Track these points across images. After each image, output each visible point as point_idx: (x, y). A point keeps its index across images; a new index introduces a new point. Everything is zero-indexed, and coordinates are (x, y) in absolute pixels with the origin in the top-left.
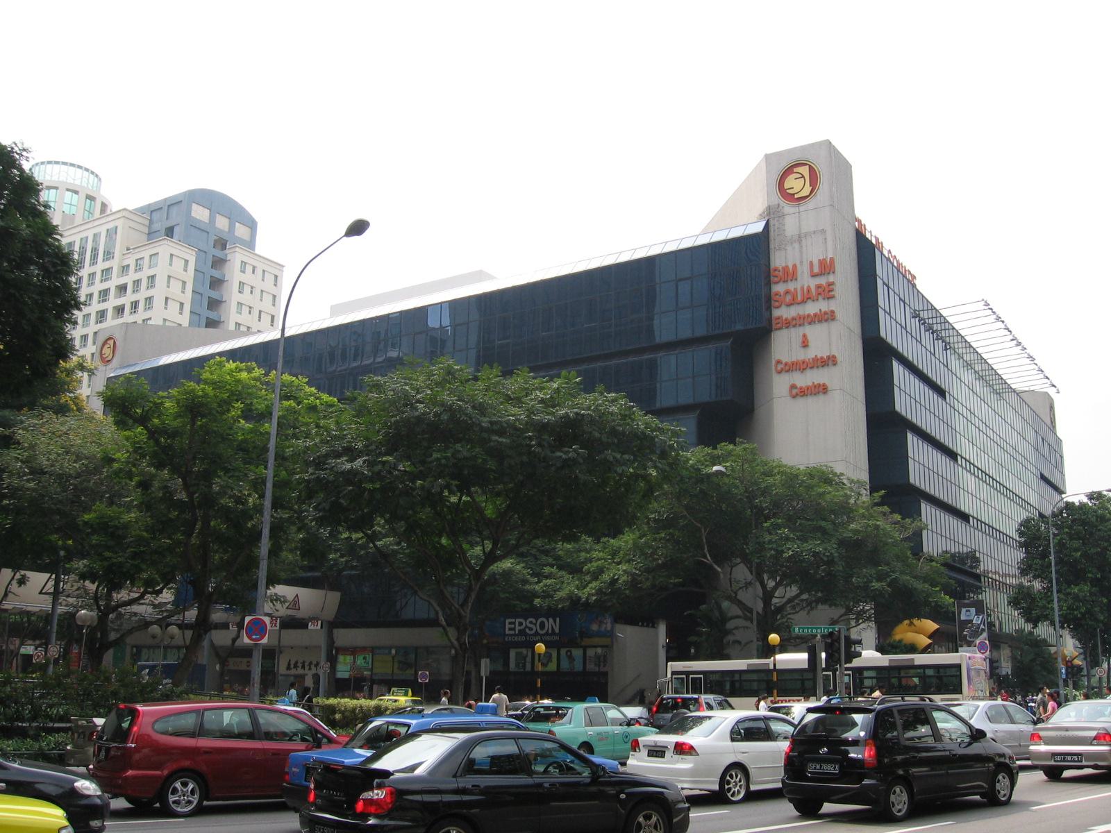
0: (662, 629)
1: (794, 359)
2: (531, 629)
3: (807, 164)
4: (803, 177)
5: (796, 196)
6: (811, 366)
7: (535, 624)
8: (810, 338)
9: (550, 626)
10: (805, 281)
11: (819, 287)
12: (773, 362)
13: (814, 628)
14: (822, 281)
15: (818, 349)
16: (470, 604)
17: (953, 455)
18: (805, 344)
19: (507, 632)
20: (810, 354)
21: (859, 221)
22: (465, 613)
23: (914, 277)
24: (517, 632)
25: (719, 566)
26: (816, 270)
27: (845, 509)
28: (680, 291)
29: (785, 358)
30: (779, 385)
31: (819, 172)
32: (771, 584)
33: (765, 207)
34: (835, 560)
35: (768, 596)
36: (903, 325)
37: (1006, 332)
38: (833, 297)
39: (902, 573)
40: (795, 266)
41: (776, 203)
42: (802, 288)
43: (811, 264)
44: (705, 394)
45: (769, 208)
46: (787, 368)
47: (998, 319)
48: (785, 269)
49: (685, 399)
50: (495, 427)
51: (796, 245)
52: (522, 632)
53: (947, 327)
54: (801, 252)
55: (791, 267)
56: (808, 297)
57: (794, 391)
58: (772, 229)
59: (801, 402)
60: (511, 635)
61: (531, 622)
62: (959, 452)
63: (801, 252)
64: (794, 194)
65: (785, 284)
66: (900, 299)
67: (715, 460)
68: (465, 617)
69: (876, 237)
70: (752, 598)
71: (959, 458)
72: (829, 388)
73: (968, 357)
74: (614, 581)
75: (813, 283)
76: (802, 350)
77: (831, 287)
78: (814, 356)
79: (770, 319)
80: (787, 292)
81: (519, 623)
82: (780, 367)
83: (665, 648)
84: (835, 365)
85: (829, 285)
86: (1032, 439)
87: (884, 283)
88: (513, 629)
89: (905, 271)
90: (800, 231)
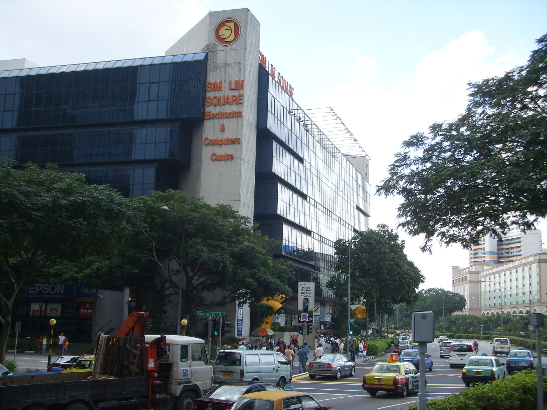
0: (127, 291)
1: (216, 138)
2: (46, 291)
3: (233, 21)
4: (231, 29)
5: (225, 40)
6: (226, 143)
7: (48, 288)
8: (225, 126)
9: (58, 290)
10: (226, 92)
11: (234, 96)
12: (204, 138)
13: (208, 313)
14: (236, 93)
15: (229, 134)
16: (13, 299)
17: (304, 196)
18: (223, 130)
19: (30, 292)
20: (225, 136)
21: (262, 55)
22: (10, 303)
23: (292, 89)
24: (36, 292)
25: (161, 263)
26: (233, 86)
27: (238, 232)
28: (151, 91)
29: (211, 137)
30: (207, 152)
31: (240, 28)
32: (191, 274)
33: (206, 44)
34: (227, 265)
35: (189, 280)
36: (282, 121)
37: (342, 125)
38: (241, 104)
39: (264, 273)
40: (221, 82)
41: (214, 43)
42: (224, 96)
43: (231, 82)
44: (162, 154)
45: (209, 45)
46: (211, 143)
47: (338, 118)
48: (215, 83)
49: (150, 156)
50: (35, 207)
51: (223, 70)
52: (40, 292)
53: (308, 120)
54: (225, 74)
55: (218, 82)
56: (227, 102)
57: (214, 157)
58: (209, 58)
59: (217, 163)
60: (32, 294)
61: (46, 286)
62: (308, 195)
63: (225, 74)
64: (224, 39)
65: (214, 92)
66: (281, 105)
67: (166, 200)
68: (10, 306)
69: (272, 66)
70: (181, 280)
71: (308, 198)
72: (235, 157)
73: (320, 137)
74: (98, 269)
75: (231, 94)
76: (221, 133)
77: (241, 97)
78: (227, 138)
79: (204, 113)
80: (215, 98)
81: (38, 286)
82: (207, 142)
83: (128, 303)
84: (239, 144)
85: (240, 96)
86: (353, 186)
87: (272, 96)
88: (34, 290)
89: (288, 85)
90: (226, 62)
